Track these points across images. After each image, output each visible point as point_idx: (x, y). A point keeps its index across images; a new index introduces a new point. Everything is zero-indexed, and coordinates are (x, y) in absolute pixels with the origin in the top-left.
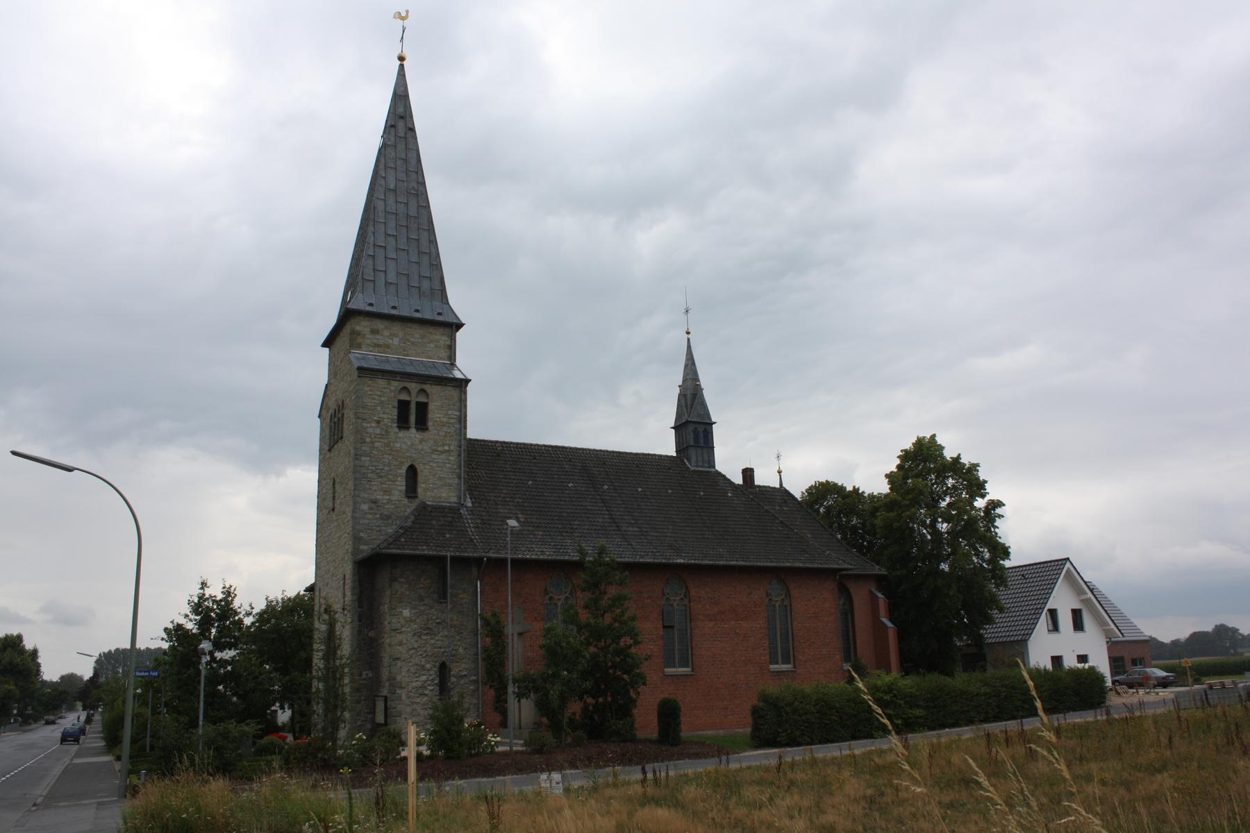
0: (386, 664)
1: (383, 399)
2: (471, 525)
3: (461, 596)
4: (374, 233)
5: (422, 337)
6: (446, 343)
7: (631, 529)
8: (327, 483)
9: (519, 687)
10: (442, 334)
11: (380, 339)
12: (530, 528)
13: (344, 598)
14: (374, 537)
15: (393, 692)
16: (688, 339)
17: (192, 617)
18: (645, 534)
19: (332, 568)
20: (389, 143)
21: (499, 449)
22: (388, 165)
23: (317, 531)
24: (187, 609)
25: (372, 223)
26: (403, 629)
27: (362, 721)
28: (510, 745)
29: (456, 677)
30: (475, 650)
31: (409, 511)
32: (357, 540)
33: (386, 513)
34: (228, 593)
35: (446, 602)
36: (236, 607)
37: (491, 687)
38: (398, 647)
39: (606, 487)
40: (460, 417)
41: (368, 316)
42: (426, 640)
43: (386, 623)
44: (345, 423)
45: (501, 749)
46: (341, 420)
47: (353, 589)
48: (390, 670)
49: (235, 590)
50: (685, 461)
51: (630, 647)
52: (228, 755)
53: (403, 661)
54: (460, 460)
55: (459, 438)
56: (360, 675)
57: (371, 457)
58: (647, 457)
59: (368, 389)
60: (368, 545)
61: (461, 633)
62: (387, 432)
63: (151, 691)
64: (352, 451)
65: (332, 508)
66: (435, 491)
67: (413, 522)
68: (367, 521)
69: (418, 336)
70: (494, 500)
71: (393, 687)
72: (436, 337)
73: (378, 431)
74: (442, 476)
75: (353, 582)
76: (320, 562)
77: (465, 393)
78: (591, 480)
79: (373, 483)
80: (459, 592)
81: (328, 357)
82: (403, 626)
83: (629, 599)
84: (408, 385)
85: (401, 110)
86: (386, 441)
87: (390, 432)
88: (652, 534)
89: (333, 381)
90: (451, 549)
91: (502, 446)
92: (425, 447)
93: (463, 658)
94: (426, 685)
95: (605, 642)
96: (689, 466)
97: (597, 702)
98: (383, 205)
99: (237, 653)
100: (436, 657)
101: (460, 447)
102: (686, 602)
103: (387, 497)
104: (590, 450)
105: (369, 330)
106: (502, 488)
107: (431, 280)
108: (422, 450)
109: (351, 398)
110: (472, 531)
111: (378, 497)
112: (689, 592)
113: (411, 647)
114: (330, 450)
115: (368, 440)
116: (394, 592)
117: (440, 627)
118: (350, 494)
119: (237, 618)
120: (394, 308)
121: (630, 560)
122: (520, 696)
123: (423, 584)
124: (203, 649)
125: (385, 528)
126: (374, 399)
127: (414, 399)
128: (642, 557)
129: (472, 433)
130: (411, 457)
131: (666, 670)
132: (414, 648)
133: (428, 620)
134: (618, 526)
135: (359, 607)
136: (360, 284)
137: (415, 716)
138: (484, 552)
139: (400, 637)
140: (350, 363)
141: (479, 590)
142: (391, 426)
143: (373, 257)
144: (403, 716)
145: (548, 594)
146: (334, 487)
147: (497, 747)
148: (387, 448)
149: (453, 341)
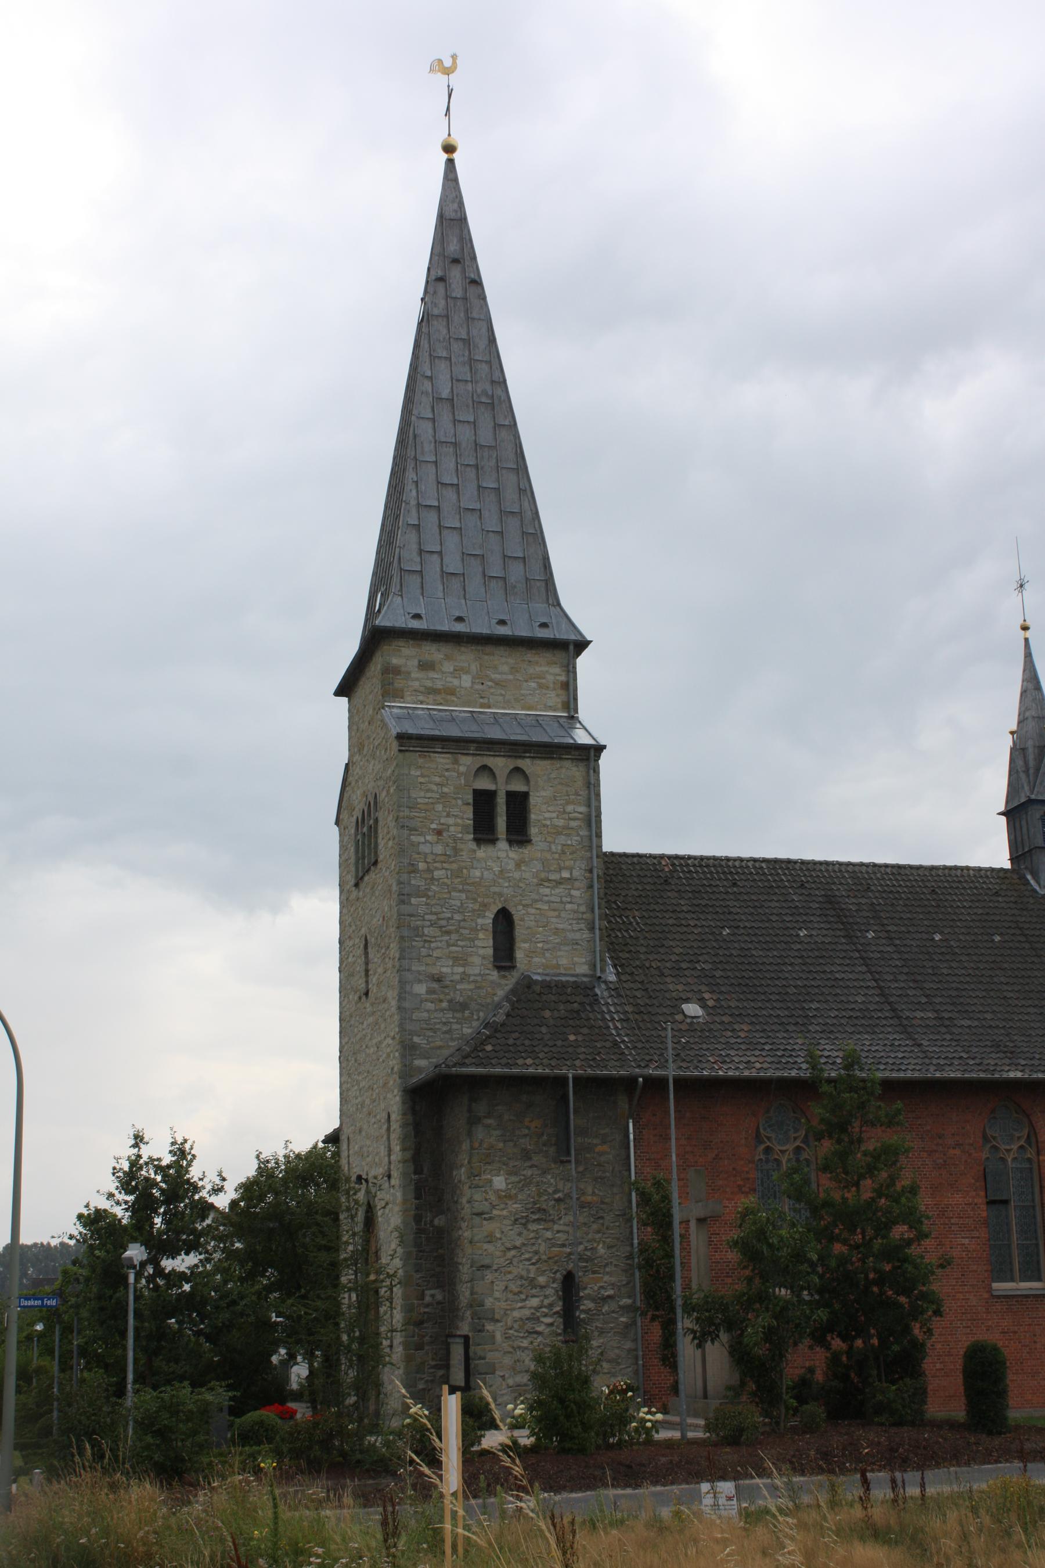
0: (465, 1277)
1: (445, 790)
2: (615, 1016)
3: (599, 1148)
4: (416, 482)
5: (514, 670)
6: (558, 678)
7: (919, 1014)
8: (354, 945)
9: (697, 1319)
10: (549, 664)
11: (435, 679)
12: (726, 1019)
13: (389, 1155)
14: (439, 1043)
15: (479, 1328)
16: (1026, 640)
17: (121, 1197)
18: (947, 1023)
19: (368, 1102)
20: (436, 312)
21: (667, 869)
22: (435, 354)
23: (340, 1033)
24: (111, 1185)
25: (413, 465)
26: (495, 1212)
27: (427, 1381)
28: (682, 1427)
29: (593, 1300)
30: (628, 1248)
31: (501, 993)
32: (408, 1049)
33: (459, 998)
34: (182, 1153)
35: (569, 1161)
36: (195, 1179)
37: (653, 1319)
38: (486, 1246)
39: (871, 935)
40: (589, 815)
41: (413, 639)
42: (536, 1231)
43: (464, 1200)
44: (380, 836)
45: (663, 1435)
46: (373, 830)
47: (404, 1139)
48: (472, 1288)
49: (192, 1148)
50: (1029, 877)
51: (909, 1243)
52: (180, 1444)
53: (496, 1271)
54: (592, 895)
55: (588, 854)
56: (422, 1297)
57: (428, 897)
58: (947, 871)
59: (418, 773)
60: (428, 1058)
61: (602, 1218)
62: (456, 850)
63: (57, 1327)
64: (394, 888)
65: (364, 990)
66: (547, 955)
67: (508, 1015)
68: (425, 1015)
69: (505, 668)
70: (658, 967)
71: (479, 1319)
72: (538, 669)
73: (439, 849)
74: (561, 926)
75: (404, 1126)
76: (348, 1090)
77: (596, 771)
78: (843, 923)
79: (433, 945)
80: (595, 1141)
81: (347, 715)
82: (494, 1207)
83: (907, 1151)
84: (490, 762)
85: (453, 247)
86: (454, 866)
87: (462, 850)
88: (963, 1023)
89: (357, 758)
90: (578, 1063)
91: (673, 865)
92: (526, 875)
93: (607, 1265)
94: (538, 1314)
95: (863, 1233)
96: (1038, 889)
97: (851, 1347)
98: (430, 431)
99: (201, 1261)
100: (556, 1262)
101: (591, 871)
102: (1031, 1153)
103: (461, 970)
104: (840, 864)
105: (416, 663)
106: (671, 943)
107: (525, 562)
108: (520, 880)
109: (388, 792)
110: (616, 1028)
111: (444, 970)
112: (1035, 1134)
113: (509, 1245)
114: (357, 885)
115: (422, 866)
116: (476, 1145)
117: (562, 1206)
118: (394, 966)
119: (197, 1197)
120: (460, 619)
121: (916, 1075)
122: (701, 1339)
123: (528, 1128)
124: (131, 1259)
125: (459, 1026)
126: (428, 791)
127: (502, 787)
128: (939, 1067)
129: (610, 845)
130: (500, 895)
131: (995, 1285)
132: (515, 1248)
133: (540, 1195)
134: (894, 1010)
135: (415, 1173)
136: (396, 580)
137: (520, 1372)
138: (639, 1066)
139: (488, 1227)
140: (384, 725)
141: (632, 1137)
142: (461, 839)
143: (417, 527)
144: (499, 1373)
145: (761, 1142)
146: (366, 953)
147: (657, 1432)
148: (457, 881)
149: (571, 675)
